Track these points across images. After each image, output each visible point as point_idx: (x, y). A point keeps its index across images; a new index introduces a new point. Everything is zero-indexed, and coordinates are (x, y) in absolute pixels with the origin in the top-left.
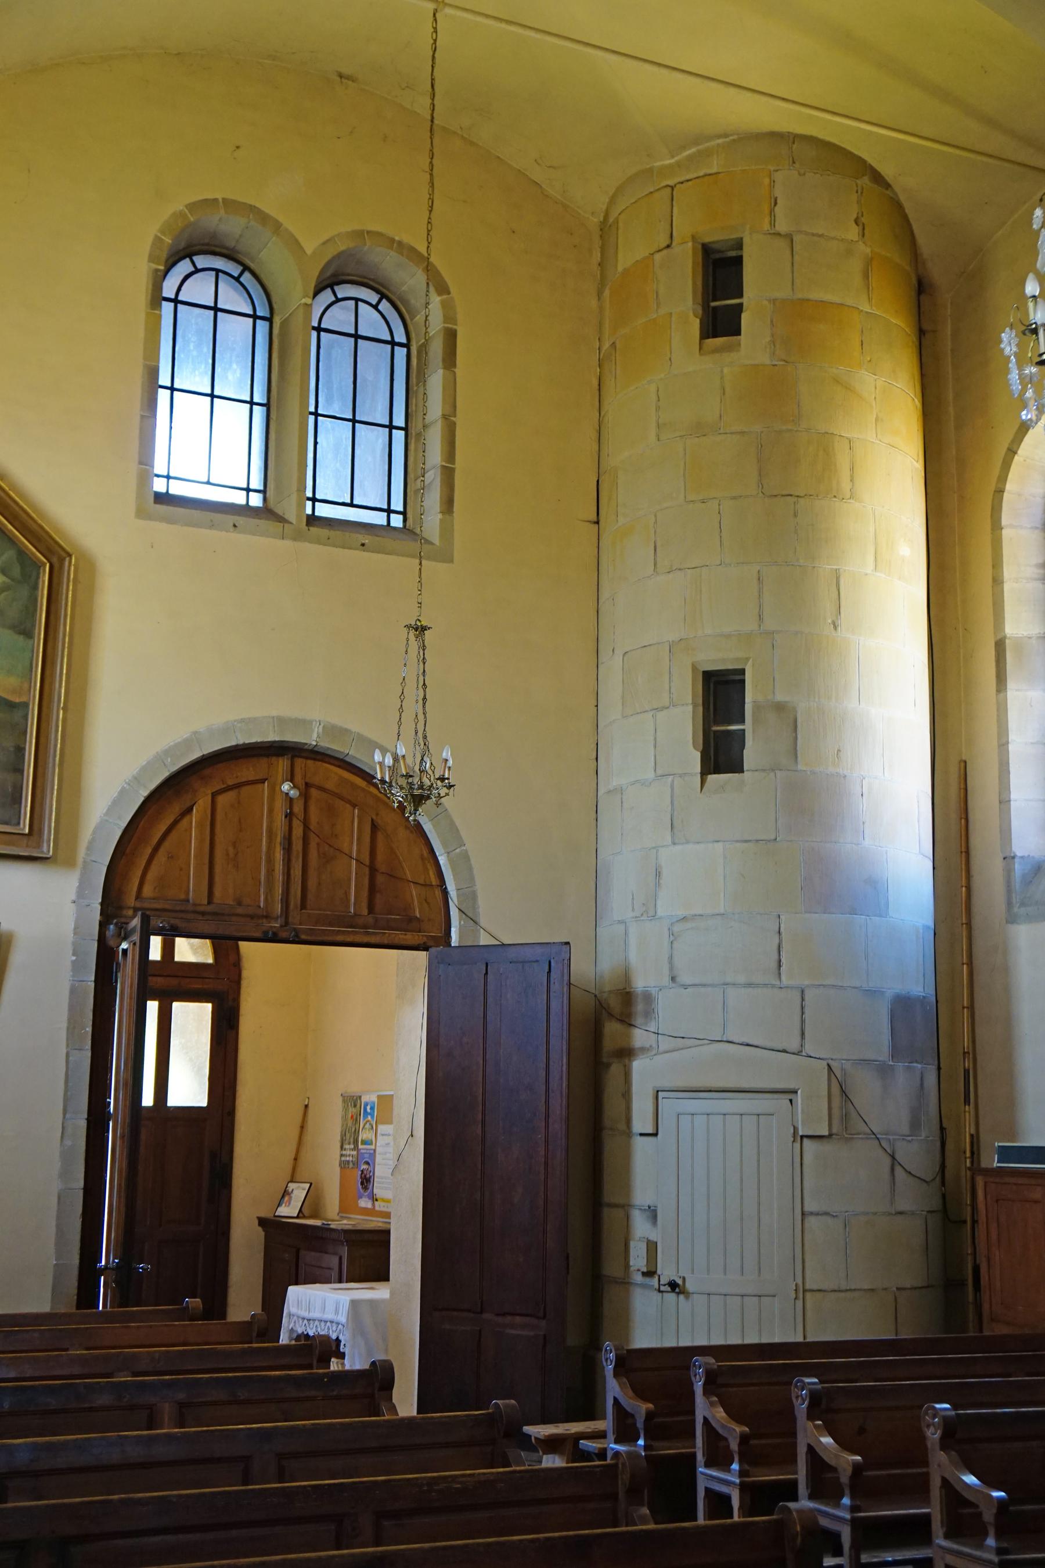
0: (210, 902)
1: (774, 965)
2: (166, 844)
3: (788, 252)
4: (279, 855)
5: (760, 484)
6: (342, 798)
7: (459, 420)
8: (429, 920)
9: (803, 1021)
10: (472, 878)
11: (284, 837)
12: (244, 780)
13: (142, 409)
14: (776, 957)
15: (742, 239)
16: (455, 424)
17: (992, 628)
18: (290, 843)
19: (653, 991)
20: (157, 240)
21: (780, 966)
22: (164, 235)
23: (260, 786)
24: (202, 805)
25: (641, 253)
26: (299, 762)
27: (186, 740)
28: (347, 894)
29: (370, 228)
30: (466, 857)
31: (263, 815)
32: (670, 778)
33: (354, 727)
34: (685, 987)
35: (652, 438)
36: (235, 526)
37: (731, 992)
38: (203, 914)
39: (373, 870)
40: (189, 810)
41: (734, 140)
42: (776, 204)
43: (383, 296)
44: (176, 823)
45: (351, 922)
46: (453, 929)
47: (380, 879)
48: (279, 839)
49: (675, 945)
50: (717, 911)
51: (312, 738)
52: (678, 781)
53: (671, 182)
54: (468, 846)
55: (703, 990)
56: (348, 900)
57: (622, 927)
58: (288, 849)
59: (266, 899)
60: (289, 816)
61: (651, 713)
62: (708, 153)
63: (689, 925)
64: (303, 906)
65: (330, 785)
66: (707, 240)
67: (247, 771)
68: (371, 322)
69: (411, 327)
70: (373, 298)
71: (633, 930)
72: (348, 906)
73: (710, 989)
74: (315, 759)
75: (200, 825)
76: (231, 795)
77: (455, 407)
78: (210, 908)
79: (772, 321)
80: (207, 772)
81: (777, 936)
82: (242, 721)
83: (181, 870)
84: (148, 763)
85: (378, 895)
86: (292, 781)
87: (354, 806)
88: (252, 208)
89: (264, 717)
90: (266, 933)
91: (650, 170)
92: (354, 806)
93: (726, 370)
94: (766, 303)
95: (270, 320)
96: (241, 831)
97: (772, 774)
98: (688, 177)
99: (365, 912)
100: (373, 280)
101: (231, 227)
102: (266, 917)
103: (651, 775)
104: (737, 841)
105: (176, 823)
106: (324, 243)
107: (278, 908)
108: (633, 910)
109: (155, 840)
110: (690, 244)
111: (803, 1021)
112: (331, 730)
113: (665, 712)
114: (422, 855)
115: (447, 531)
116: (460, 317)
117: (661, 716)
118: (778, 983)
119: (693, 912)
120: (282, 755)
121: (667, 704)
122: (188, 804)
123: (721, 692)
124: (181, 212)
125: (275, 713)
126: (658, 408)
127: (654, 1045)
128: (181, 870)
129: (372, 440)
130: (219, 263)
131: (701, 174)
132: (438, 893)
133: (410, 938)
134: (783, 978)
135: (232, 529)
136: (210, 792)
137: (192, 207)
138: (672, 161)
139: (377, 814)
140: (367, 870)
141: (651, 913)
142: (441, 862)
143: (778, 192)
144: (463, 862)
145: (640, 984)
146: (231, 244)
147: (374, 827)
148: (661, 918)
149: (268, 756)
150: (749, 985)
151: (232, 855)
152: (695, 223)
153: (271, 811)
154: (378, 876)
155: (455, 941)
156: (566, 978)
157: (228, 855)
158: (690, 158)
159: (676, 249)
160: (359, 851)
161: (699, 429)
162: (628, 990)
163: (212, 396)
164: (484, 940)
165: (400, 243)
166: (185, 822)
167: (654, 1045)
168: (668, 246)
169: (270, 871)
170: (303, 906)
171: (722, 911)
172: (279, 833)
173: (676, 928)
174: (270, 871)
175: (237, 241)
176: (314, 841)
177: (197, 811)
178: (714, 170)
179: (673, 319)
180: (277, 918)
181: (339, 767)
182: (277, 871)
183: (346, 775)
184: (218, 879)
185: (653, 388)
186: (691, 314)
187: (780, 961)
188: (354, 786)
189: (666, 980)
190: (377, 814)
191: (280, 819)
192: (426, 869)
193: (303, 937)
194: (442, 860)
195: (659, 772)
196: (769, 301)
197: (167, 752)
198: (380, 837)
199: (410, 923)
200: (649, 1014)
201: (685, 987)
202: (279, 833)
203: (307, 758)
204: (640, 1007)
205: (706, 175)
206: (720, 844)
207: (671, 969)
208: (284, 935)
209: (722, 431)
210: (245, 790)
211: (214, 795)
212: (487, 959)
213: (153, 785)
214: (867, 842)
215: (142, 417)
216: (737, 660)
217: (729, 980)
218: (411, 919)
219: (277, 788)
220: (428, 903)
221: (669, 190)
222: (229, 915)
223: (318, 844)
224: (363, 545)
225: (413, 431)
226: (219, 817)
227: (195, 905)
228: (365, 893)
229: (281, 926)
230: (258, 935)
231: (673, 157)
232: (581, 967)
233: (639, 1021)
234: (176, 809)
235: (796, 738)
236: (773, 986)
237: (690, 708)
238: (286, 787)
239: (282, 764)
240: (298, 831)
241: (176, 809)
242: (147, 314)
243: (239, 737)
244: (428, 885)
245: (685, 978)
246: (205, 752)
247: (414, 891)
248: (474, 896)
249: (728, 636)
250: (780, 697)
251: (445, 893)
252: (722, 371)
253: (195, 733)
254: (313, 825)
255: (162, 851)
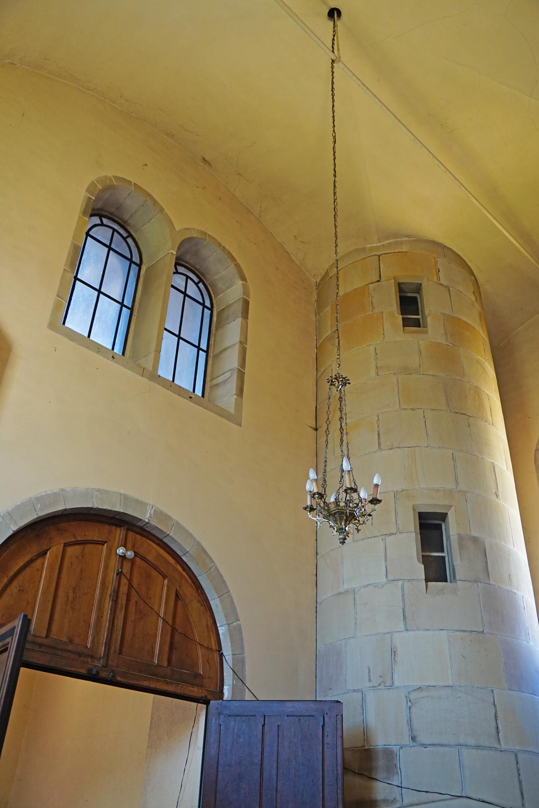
0: (47, 637)
1: (494, 731)
2: (20, 577)
3: (448, 293)
4: (108, 604)
5: (448, 404)
6: (156, 569)
7: (248, 346)
8: (209, 678)
9: (520, 782)
10: (242, 648)
11: (114, 591)
12: (89, 538)
13: (65, 265)
14: (494, 724)
15: (421, 285)
16: (246, 349)
17: (459, 555)
18: (117, 597)
19: (395, 749)
20: (93, 184)
21: (498, 733)
22: (98, 183)
23: (101, 546)
24: (56, 550)
25: (358, 284)
26: (131, 535)
27: (55, 495)
28: (153, 648)
29: (210, 233)
30: (239, 628)
31: (99, 570)
32: (400, 583)
33: (175, 516)
34: (425, 746)
35: (373, 373)
36: (113, 357)
37: (465, 752)
38: (41, 645)
39: (174, 629)
40: (44, 553)
41: (414, 240)
42: (439, 271)
43: (201, 280)
44: (31, 561)
45: (152, 671)
46: (226, 688)
47: (177, 637)
48: (109, 592)
49: (413, 710)
50: (447, 684)
51: (146, 516)
52: (406, 584)
53: (379, 253)
54: (241, 622)
55: (441, 749)
56: (153, 652)
57: (359, 695)
58: (115, 601)
59: (93, 641)
60: (120, 574)
61: (382, 537)
62: (401, 243)
63: (424, 694)
64: (120, 653)
65: (150, 557)
66: (401, 281)
67: (93, 532)
68: (192, 290)
69: (214, 301)
70: (196, 280)
71: (371, 697)
72: (153, 657)
73: (446, 749)
74: (142, 535)
75: (51, 568)
76: (77, 549)
77: (247, 339)
78: (45, 641)
79: (444, 324)
80: (63, 525)
81: (493, 707)
82: (99, 490)
83: (28, 603)
84: (22, 504)
85: (174, 652)
86: (125, 547)
87: (164, 577)
88: (149, 195)
89: (114, 492)
90: (90, 670)
91: (364, 249)
92: (164, 577)
93: (421, 342)
94: (439, 314)
95: (140, 266)
96: (81, 579)
97: (475, 585)
98: (389, 252)
99: (165, 664)
100: (197, 270)
101: (131, 204)
102: (91, 657)
103: (384, 580)
104: (457, 631)
105: (31, 561)
106: (186, 229)
107: (102, 650)
108: (370, 680)
109: (12, 573)
110: (393, 281)
111: (520, 782)
112: (158, 514)
113: (393, 536)
114: (207, 625)
115: (239, 406)
116: (251, 295)
117: (389, 539)
118: (498, 746)
119: (427, 684)
120: (120, 526)
121: (395, 532)
122: (45, 548)
123: (430, 528)
124: (110, 177)
125: (122, 492)
126: (376, 359)
127: (399, 798)
128: (28, 603)
129: (187, 353)
130: (116, 227)
131: (397, 251)
132: (216, 656)
133: (195, 691)
134: (502, 742)
135: (111, 358)
136: (63, 542)
137: (116, 178)
138: (379, 244)
139: (180, 587)
140: (169, 629)
141: (389, 683)
142: (220, 632)
143: (439, 266)
144: (236, 633)
145: (380, 741)
146: (126, 217)
147: (177, 596)
148: (398, 688)
149: (110, 524)
150: (478, 747)
151: (71, 598)
152: (392, 272)
153: (106, 568)
154: (178, 636)
155: (227, 695)
156: (339, 733)
157: (68, 597)
158: (390, 244)
159: (383, 283)
160: (165, 613)
161: (406, 370)
162: (366, 747)
163: (99, 292)
164: (248, 696)
165: (224, 247)
166: (39, 561)
167: (399, 798)
168: (378, 281)
169: (99, 618)
170: (120, 653)
171: (451, 684)
172: (110, 587)
173: (413, 696)
174: (99, 618)
175: (131, 216)
176: (134, 597)
177: (50, 554)
178: (405, 251)
179: (384, 315)
180: (99, 659)
181: (158, 545)
182: (104, 619)
183: (162, 552)
184: (57, 616)
185: (372, 349)
186: (396, 313)
187: (498, 728)
188: (168, 562)
189: (407, 740)
190: (180, 587)
191: (112, 575)
192: (209, 637)
193: (119, 679)
194: (222, 630)
195: (390, 578)
196: (442, 314)
197: (39, 499)
198: (179, 603)
199: (196, 679)
200: (392, 768)
201: (425, 746)
202: (110, 587)
203: (137, 533)
204: (381, 762)
205: (399, 252)
206: (445, 632)
207: (411, 729)
208: (103, 674)
209: (421, 373)
210: (89, 547)
211: (66, 545)
212: (260, 714)
213: (22, 523)
214: (531, 643)
215: (65, 270)
216: (445, 506)
217: (462, 741)
218: (197, 675)
219: (113, 551)
220: (209, 663)
221: (378, 257)
222: (63, 650)
223: (136, 602)
224: (191, 397)
225: (211, 354)
226: (66, 564)
227: (34, 636)
228: (167, 648)
229: (103, 666)
230: (83, 671)
231: (379, 242)
232: (350, 720)
233: (380, 775)
234: (35, 549)
235: (487, 562)
236: (496, 749)
237: (414, 534)
238: (121, 551)
239: (119, 533)
240: (124, 589)
241: (35, 549)
242: (80, 218)
243: (95, 502)
244: (209, 649)
245: (423, 738)
246: (68, 507)
247: (200, 652)
248: (243, 661)
249: (438, 490)
250: (474, 534)
251: (221, 655)
252: (419, 343)
253: (63, 490)
254: (135, 583)
255: (15, 583)
